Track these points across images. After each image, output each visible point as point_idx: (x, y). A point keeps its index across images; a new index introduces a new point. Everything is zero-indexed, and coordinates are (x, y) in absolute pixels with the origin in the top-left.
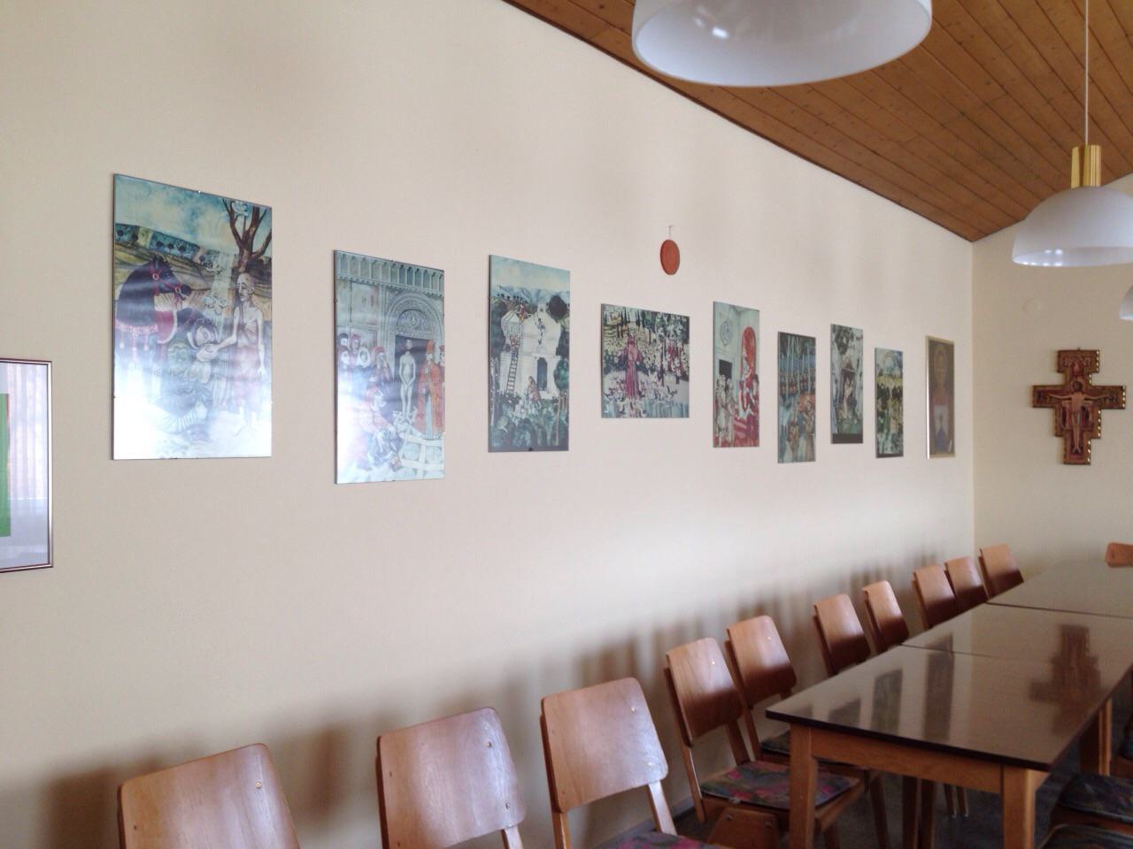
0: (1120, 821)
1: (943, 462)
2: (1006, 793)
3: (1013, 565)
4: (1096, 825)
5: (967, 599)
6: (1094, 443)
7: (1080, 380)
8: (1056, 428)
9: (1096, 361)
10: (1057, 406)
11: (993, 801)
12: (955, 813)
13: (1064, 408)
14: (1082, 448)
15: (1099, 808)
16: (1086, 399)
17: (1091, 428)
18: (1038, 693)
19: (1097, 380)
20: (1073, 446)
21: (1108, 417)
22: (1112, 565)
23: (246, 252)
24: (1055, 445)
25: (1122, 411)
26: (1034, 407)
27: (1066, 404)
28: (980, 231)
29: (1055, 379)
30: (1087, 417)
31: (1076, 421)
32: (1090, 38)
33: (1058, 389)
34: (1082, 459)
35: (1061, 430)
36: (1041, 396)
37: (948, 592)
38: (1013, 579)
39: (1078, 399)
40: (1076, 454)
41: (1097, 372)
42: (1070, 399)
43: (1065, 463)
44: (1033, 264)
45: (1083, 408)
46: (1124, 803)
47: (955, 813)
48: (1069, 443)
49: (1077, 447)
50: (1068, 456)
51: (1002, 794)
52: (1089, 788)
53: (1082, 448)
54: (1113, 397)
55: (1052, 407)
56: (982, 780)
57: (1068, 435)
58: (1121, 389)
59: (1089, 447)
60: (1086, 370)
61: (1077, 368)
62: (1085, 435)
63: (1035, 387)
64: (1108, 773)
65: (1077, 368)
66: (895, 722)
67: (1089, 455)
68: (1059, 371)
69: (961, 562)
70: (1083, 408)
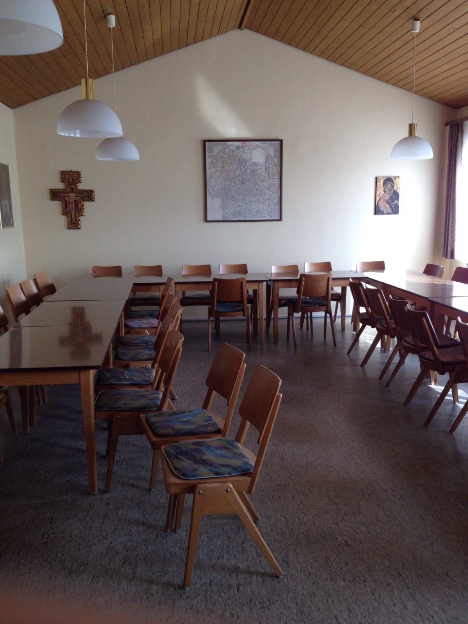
0: (123, 385)
1: (8, 230)
2: (82, 382)
3: (50, 281)
4: (114, 388)
5: (34, 301)
6: (81, 218)
7: (73, 186)
8: (63, 211)
9: (80, 177)
10: (63, 200)
11: (76, 388)
12: (41, 402)
13: (66, 201)
14: (76, 221)
15: (114, 381)
16: (76, 196)
17: (80, 211)
18: (63, 341)
19: (81, 187)
20: (72, 220)
21: (86, 204)
22: (95, 277)
23: (328, 315)
24: (63, 220)
25: (93, 202)
26: (52, 200)
27: (66, 198)
28: (17, 104)
29: (60, 186)
30: (77, 206)
31: (72, 207)
32: (84, 21)
33: (63, 191)
34: (77, 226)
35: (66, 212)
36: (55, 195)
37: (23, 298)
38: (51, 289)
39: (72, 195)
40: (74, 224)
41: (81, 183)
42: (69, 196)
43: (69, 229)
44: (66, 135)
45: (75, 201)
46: (122, 377)
47: (41, 402)
48: (70, 219)
49: (74, 220)
50: (70, 224)
51: (80, 383)
52: (108, 374)
53: (76, 221)
54: (89, 195)
55: (60, 200)
56: (71, 378)
57: (69, 215)
58: (92, 191)
59: (79, 220)
60: (75, 181)
61: (71, 180)
62: (77, 215)
63: (51, 189)
64: (112, 367)
65: (71, 180)
66: (20, 362)
67: (79, 224)
68: (62, 182)
69: (26, 282)
70: (75, 201)
